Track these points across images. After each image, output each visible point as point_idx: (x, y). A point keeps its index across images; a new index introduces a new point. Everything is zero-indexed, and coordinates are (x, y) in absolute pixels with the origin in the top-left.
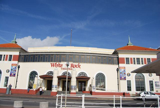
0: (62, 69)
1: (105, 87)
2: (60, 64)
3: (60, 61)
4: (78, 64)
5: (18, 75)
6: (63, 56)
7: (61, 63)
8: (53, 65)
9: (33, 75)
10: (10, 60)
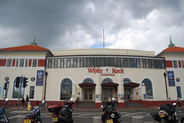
0: (103, 75)
1: (152, 95)
2: (99, 70)
3: (100, 66)
4: (120, 69)
5: (166, 84)
6: (95, 59)
7: (101, 68)
8: (91, 70)
9: (66, 84)
10: (35, 65)
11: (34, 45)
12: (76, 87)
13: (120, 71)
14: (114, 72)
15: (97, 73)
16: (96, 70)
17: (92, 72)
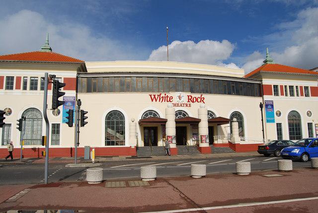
2: (167, 97)
3: (170, 89)
7: (170, 94)
8: (155, 97)
9: (115, 121)
11: (48, 51)
13: (199, 100)
17: (156, 101)
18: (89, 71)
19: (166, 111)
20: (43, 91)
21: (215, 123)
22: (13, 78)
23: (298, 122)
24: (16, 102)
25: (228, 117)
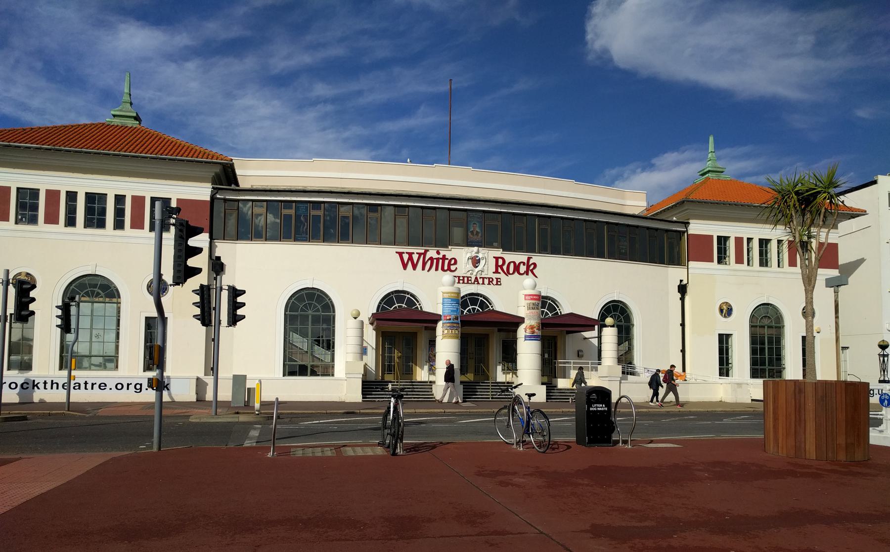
2: (444, 258)
3: (446, 243)
6: (228, 203)
7: (451, 253)
8: (410, 258)
9: (309, 313)
11: (131, 123)
12: (362, 322)
13: (523, 269)
14: (500, 270)
15: (437, 269)
16: (431, 259)
17: (414, 267)
18: (244, 184)
19: (433, 292)
20: (153, 234)
21: (559, 331)
22: (35, 193)
23: (773, 332)
24: (54, 255)
25: (595, 316)
